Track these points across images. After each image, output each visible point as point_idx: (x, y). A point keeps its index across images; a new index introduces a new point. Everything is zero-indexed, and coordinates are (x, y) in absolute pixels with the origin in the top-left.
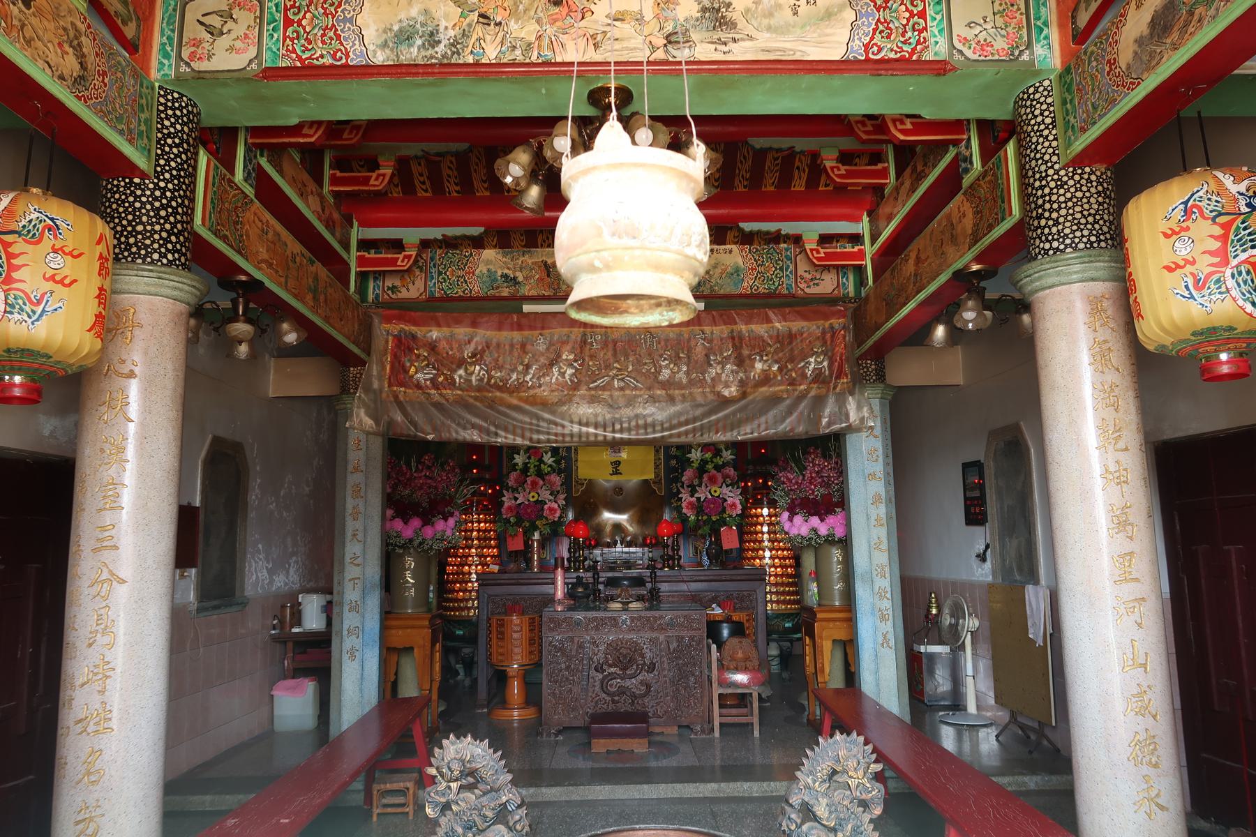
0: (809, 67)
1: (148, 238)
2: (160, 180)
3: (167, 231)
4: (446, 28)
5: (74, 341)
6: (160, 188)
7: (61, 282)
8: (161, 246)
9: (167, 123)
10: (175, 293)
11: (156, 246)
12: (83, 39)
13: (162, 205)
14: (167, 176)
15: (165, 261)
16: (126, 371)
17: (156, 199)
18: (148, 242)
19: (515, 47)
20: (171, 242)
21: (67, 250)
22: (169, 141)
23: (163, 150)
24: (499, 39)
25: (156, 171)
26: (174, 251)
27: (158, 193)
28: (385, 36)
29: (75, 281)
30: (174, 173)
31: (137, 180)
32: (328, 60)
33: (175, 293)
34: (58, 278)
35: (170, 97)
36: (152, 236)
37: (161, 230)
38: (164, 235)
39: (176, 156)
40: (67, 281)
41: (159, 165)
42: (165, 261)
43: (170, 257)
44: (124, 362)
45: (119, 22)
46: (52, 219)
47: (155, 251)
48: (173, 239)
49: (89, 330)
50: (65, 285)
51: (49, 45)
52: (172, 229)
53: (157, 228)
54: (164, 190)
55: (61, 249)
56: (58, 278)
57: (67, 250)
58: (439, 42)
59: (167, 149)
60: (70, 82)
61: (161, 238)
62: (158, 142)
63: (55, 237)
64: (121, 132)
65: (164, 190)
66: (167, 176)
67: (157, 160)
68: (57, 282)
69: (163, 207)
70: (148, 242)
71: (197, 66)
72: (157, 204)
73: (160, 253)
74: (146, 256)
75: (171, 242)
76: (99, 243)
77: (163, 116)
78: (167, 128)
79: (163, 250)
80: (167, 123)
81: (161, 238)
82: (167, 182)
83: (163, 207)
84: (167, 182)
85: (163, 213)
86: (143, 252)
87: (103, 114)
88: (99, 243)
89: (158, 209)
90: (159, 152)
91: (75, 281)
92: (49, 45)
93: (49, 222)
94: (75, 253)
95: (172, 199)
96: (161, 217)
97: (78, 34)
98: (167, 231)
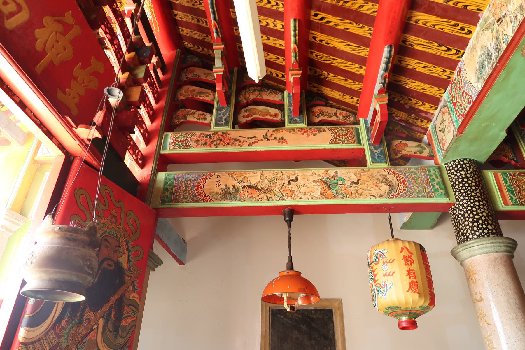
0: (35, 119)
1: (465, 230)
2: (459, 202)
3: (471, 222)
4: (491, 44)
5: (403, 298)
6: (461, 205)
7: (389, 275)
8: (471, 231)
9: (453, 176)
10: (485, 250)
11: (469, 232)
12: (388, 176)
13: (464, 212)
14: (462, 198)
15: (475, 237)
16: (478, 298)
17: (461, 211)
18: (465, 232)
19: (516, 16)
20: (475, 226)
21: (388, 261)
22: (457, 183)
23: (456, 189)
24: (509, 22)
25: (456, 199)
26: (478, 230)
27: (461, 208)
28: (477, 75)
29: (394, 272)
30: (464, 194)
31: (453, 207)
32: (469, 106)
33: (485, 250)
34: (387, 274)
35: (450, 165)
36: (466, 228)
37: (468, 223)
38: (471, 225)
39: (462, 187)
40: (391, 274)
41: (457, 195)
42: (475, 237)
43: (477, 233)
44: (476, 294)
45: (418, 154)
46: (381, 252)
47: (469, 234)
48: (476, 224)
49: (409, 290)
50: (390, 276)
51: (372, 189)
52: (473, 220)
53: (466, 223)
54: (463, 205)
55: (386, 262)
56: (387, 274)
57: (388, 261)
58: (492, 54)
59: (457, 187)
60: (385, 195)
61: (470, 227)
62: (453, 186)
63: (383, 258)
64: (423, 196)
65: (463, 205)
66: (462, 198)
67: (455, 194)
68: (387, 276)
69: (465, 212)
70: (465, 232)
71: (445, 148)
72: (462, 213)
73: (472, 234)
74: (467, 238)
75: (475, 226)
76: (401, 252)
77: (450, 174)
78: (454, 178)
79: (473, 232)
80: (453, 176)
81: (470, 227)
82: (463, 200)
83: (465, 212)
84: (463, 200)
85: (466, 215)
86: (465, 237)
87: (408, 196)
88: (401, 252)
89: (464, 215)
90: (455, 190)
91: (394, 272)
92: (372, 189)
93: (380, 253)
94: (391, 261)
95: (468, 207)
96: (466, 217)
97: (384, 176)
98: (471, 222)
